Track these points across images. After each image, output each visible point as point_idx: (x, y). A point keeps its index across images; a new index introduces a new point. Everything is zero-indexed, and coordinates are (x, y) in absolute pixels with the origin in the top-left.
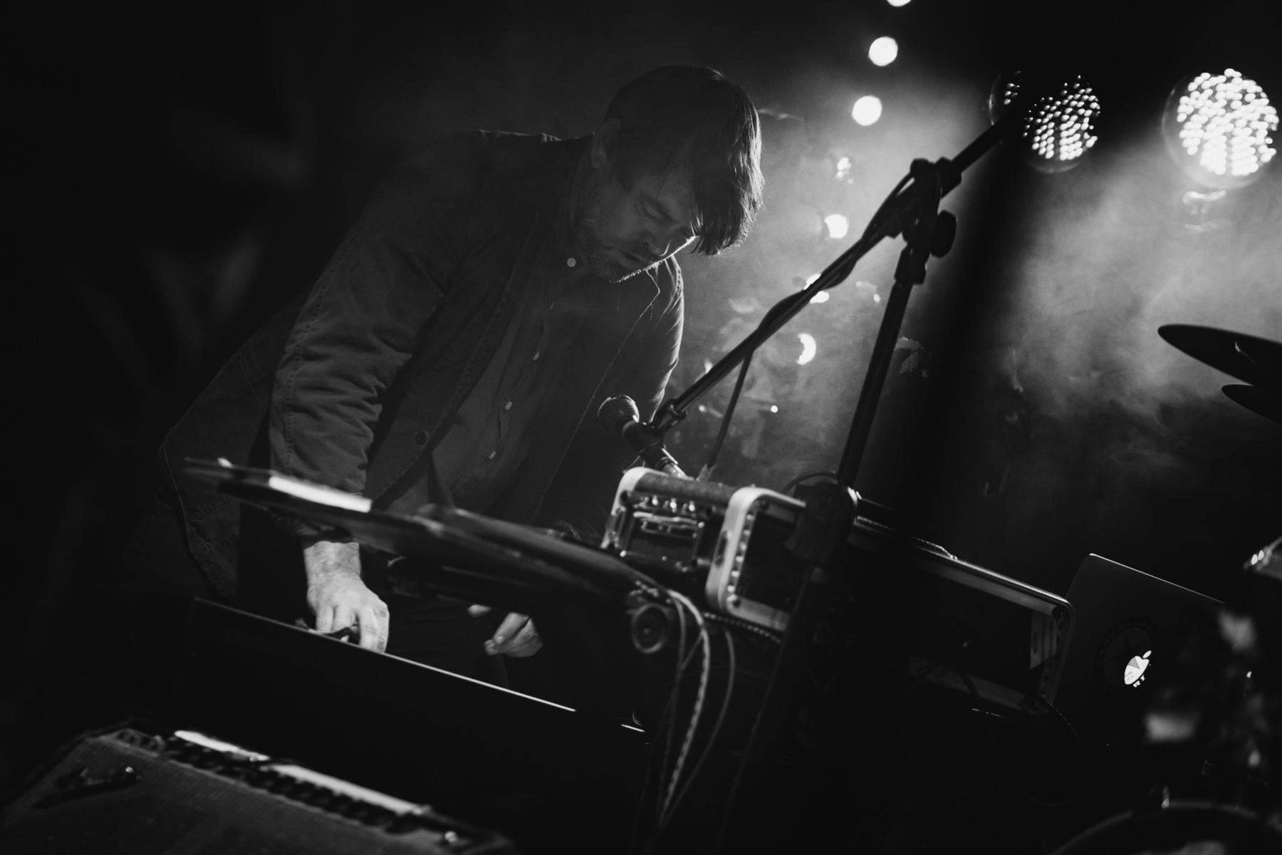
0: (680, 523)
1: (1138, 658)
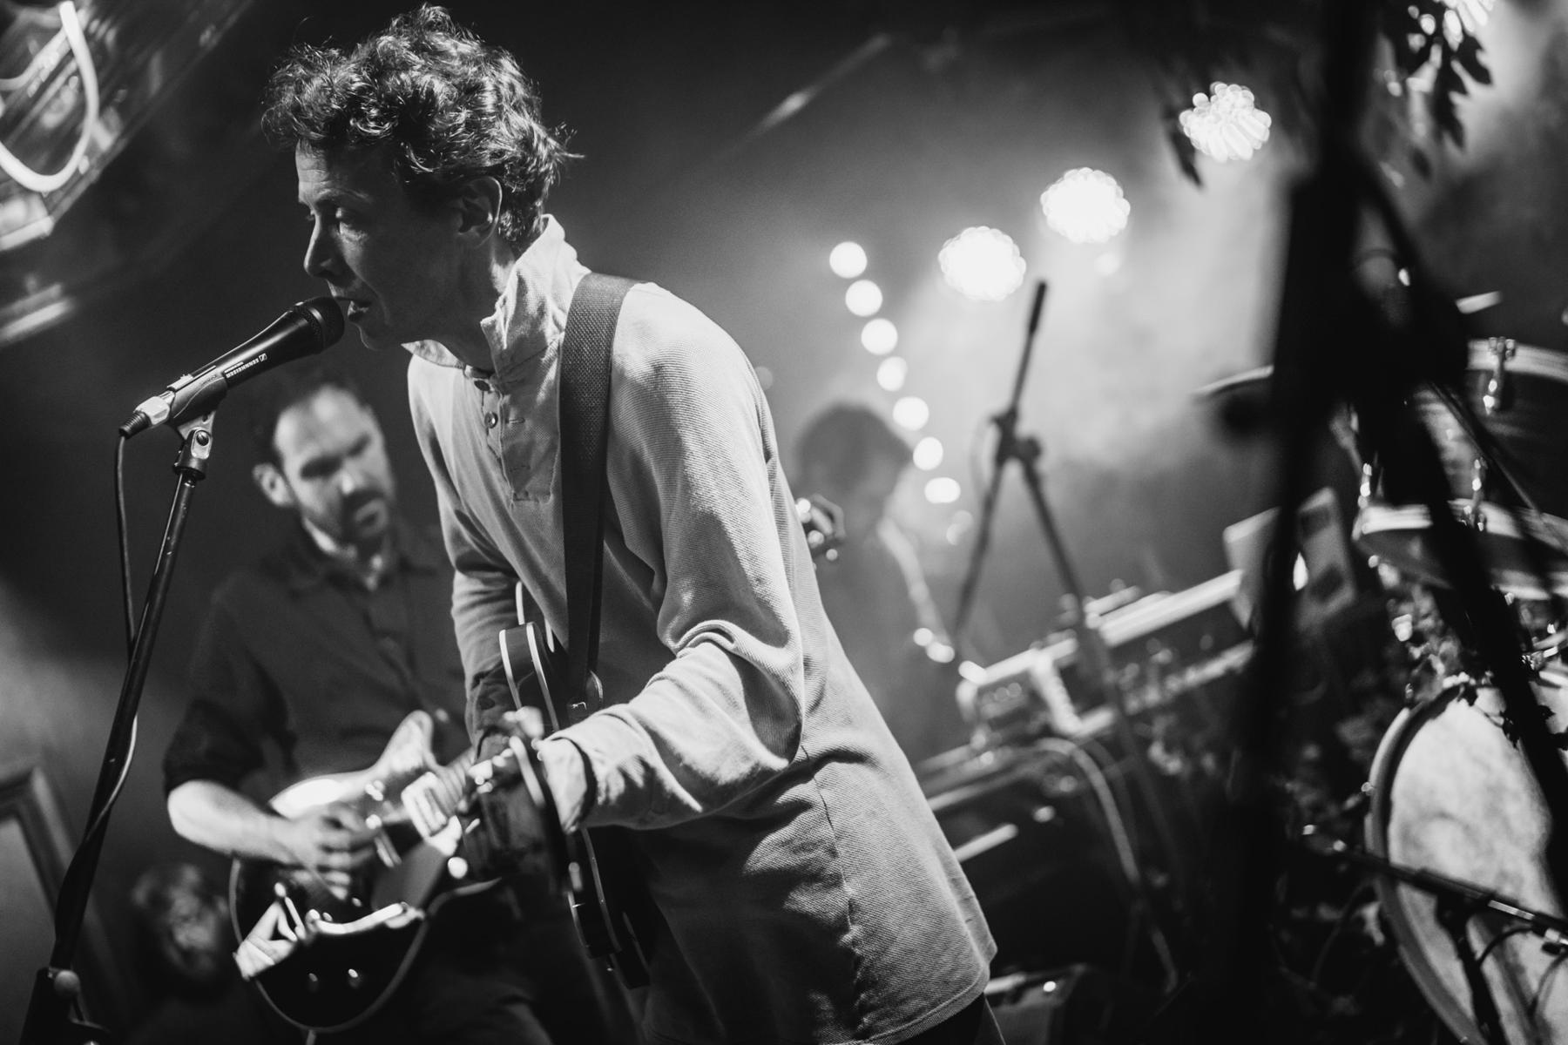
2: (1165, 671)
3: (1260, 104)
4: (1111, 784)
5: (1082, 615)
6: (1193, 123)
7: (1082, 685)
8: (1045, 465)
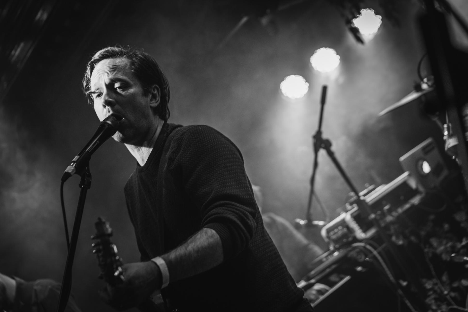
3: (376, 13)
4: (379, 253)
5: (359, 197)
6: (356, 22)
8: (334, 148)
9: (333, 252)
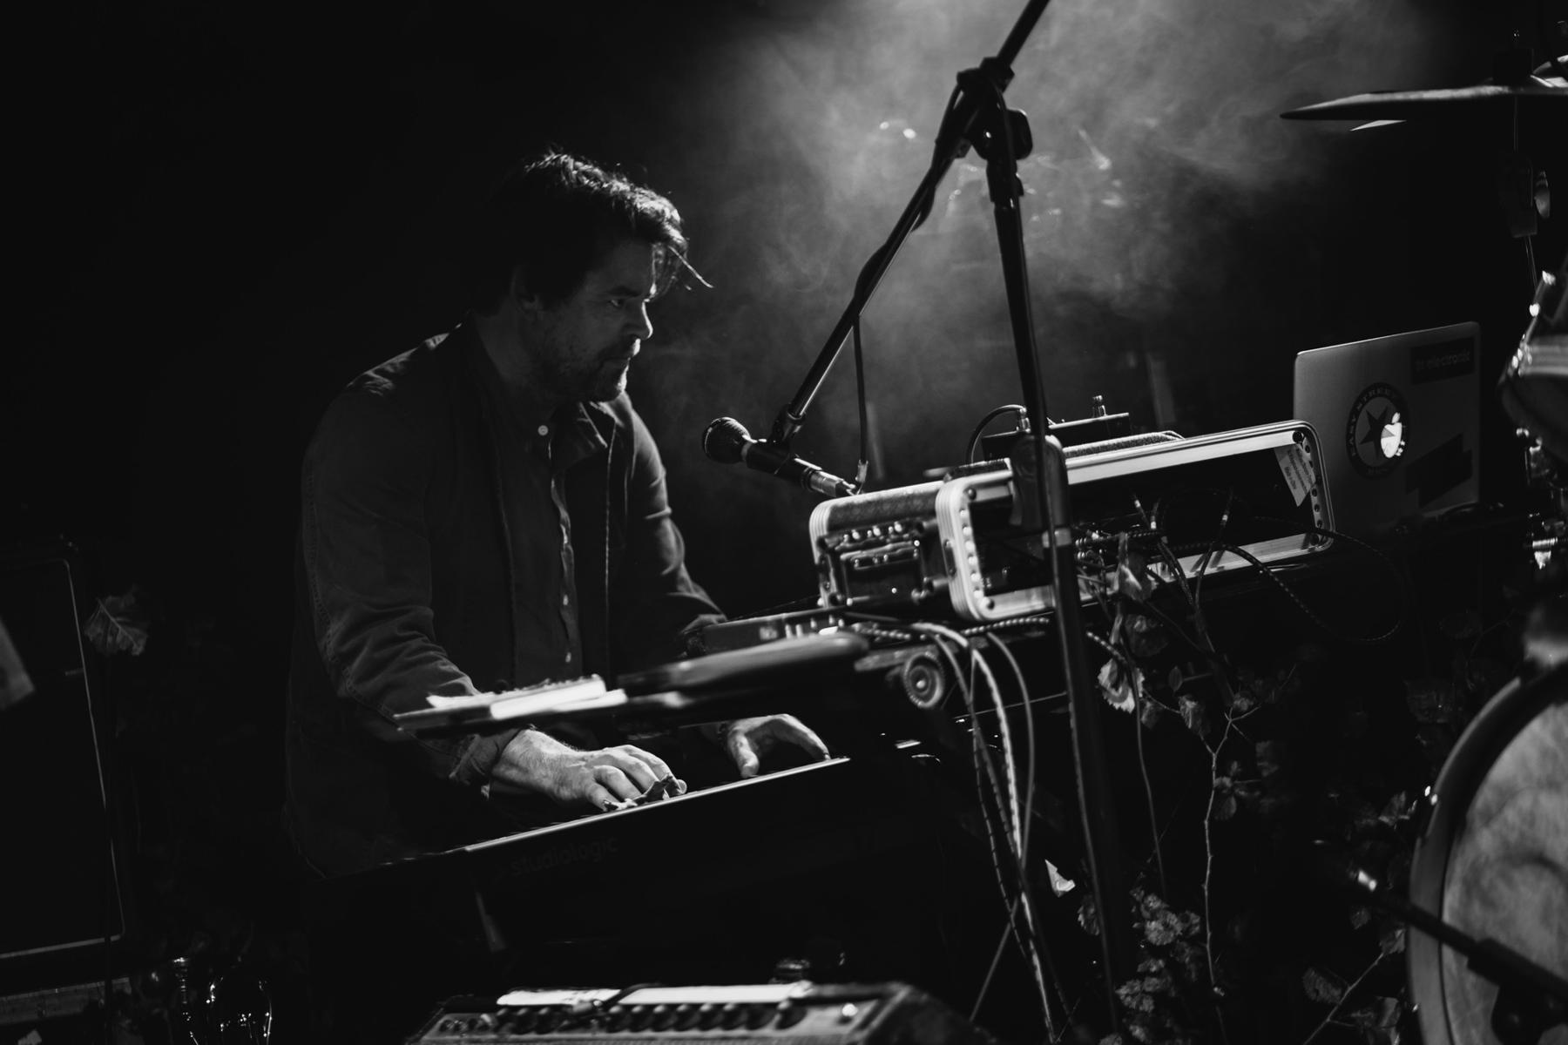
0: (894, 549)
1: (1388, 427)
2: (1143, 552)
7: (1006, 544)
9: (822, 620)
